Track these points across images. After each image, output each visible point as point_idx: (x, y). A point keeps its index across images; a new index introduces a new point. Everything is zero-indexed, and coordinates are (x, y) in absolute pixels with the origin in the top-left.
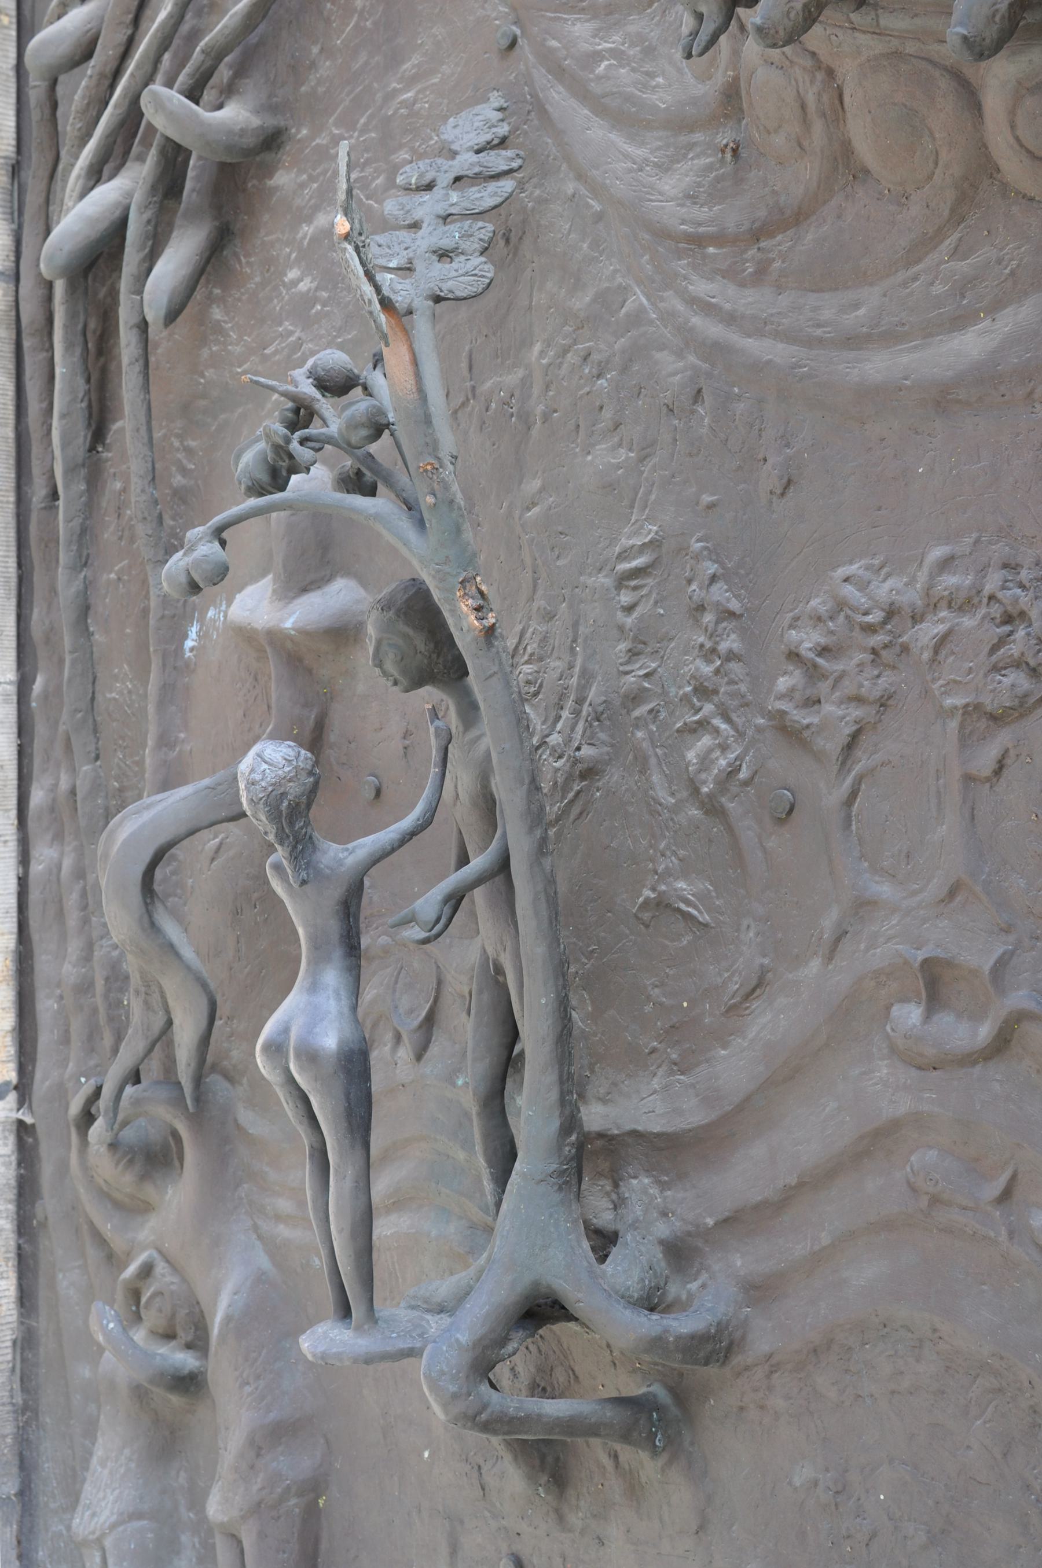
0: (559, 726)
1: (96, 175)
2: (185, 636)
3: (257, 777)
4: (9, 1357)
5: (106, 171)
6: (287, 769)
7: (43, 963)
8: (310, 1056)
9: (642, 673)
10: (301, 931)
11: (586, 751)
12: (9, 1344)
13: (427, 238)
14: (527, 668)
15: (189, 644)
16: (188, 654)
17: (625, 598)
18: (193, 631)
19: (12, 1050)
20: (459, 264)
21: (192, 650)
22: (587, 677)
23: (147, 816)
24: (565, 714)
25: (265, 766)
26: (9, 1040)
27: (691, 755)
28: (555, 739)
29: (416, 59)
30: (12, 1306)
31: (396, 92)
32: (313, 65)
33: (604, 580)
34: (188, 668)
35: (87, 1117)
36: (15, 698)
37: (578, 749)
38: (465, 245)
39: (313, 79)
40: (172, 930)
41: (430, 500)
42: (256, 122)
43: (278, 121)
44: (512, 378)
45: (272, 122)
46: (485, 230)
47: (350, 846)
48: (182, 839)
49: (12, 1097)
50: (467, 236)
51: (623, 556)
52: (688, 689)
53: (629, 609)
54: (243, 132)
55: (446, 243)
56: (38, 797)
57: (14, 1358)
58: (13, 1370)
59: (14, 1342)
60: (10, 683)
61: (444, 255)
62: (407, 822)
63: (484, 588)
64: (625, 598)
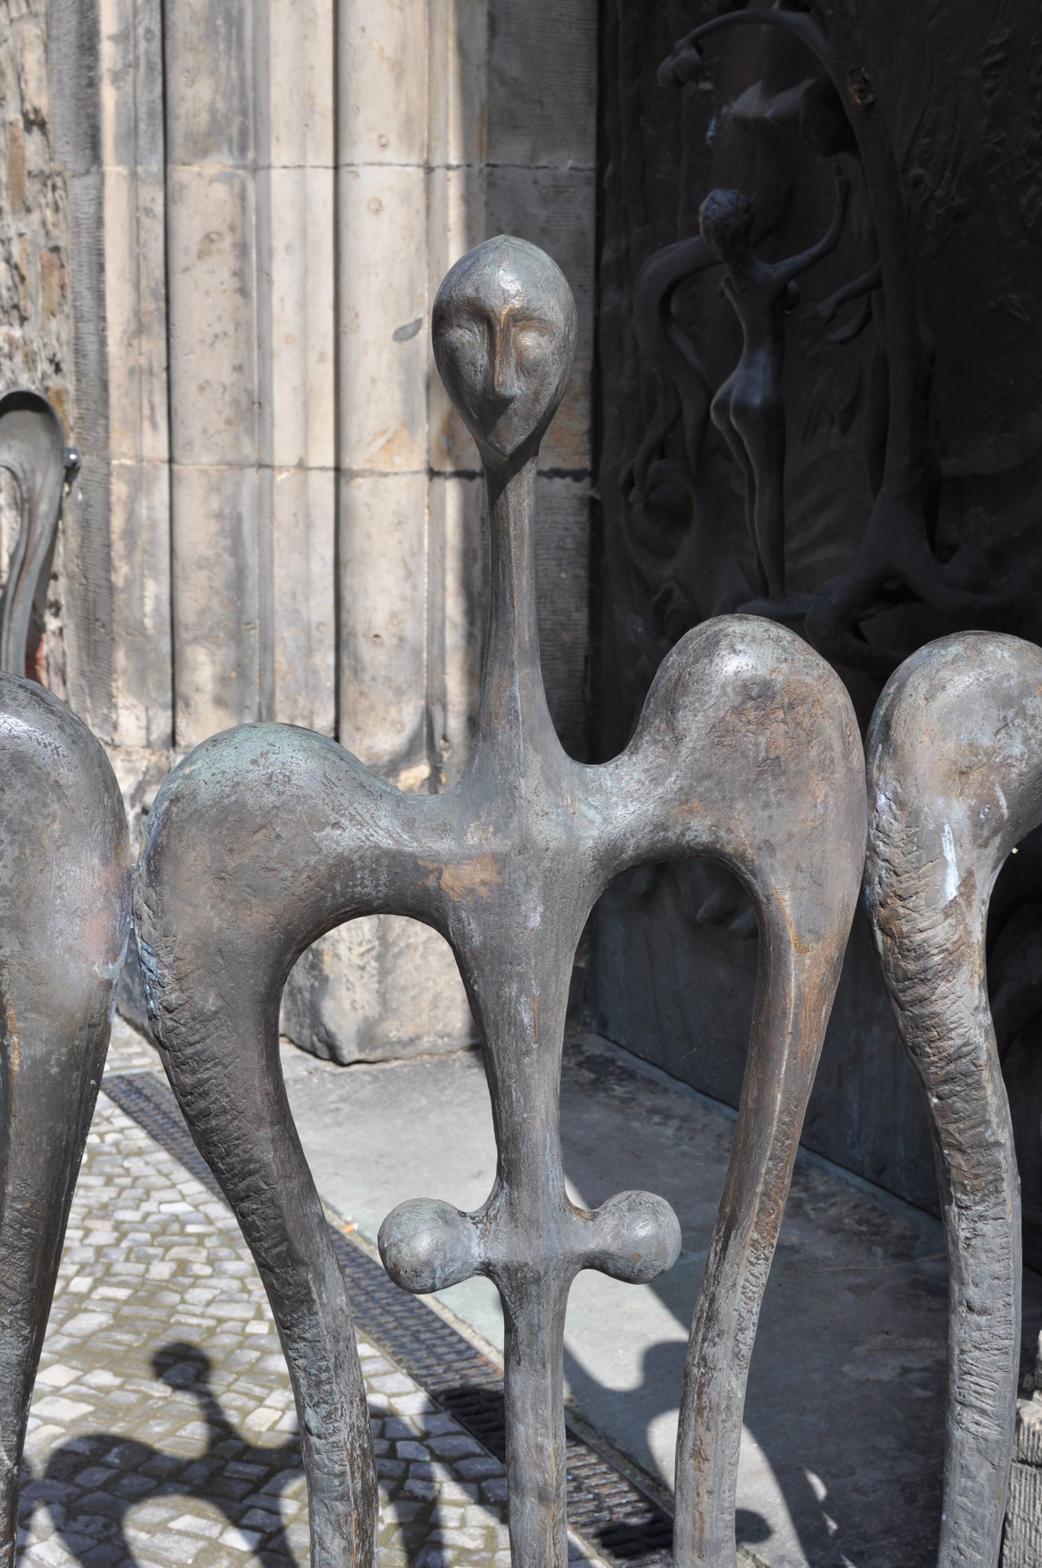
0: (943, 183)
2: (707, 129)
3: (709, 213)
4: (582, 668)
6: (730, 208)
8: (742, 410)
9: (996, 140)
10: (743, 325)
12: (582, 658)
14: (925, 141)
15: (710, 133)
16: (709, 142)
17: (988, 85)
18: (713, 124)
19: (588, 447)
21: (712, 138)
24: (947, 174)
25: (715, 206)
26: (585, 438)
27: (1024, 201)
28: (940, 193)
30: (585, 632)
35: (630, 483)
36: (594, 181)
37: (953, 199)
40: (683, 343)
41: (830, 12)
47: (776, 265)
48: (430, 99)
49: (587, 481)
52: (1024, 151)
53: (990, 93)
56: (607, 254)
57: (586, 671)
58: (585, 677)
59: (586, 658)
60: (591, 170)
62: (815, 249)
63: (866, 76)
64: (988, 85)
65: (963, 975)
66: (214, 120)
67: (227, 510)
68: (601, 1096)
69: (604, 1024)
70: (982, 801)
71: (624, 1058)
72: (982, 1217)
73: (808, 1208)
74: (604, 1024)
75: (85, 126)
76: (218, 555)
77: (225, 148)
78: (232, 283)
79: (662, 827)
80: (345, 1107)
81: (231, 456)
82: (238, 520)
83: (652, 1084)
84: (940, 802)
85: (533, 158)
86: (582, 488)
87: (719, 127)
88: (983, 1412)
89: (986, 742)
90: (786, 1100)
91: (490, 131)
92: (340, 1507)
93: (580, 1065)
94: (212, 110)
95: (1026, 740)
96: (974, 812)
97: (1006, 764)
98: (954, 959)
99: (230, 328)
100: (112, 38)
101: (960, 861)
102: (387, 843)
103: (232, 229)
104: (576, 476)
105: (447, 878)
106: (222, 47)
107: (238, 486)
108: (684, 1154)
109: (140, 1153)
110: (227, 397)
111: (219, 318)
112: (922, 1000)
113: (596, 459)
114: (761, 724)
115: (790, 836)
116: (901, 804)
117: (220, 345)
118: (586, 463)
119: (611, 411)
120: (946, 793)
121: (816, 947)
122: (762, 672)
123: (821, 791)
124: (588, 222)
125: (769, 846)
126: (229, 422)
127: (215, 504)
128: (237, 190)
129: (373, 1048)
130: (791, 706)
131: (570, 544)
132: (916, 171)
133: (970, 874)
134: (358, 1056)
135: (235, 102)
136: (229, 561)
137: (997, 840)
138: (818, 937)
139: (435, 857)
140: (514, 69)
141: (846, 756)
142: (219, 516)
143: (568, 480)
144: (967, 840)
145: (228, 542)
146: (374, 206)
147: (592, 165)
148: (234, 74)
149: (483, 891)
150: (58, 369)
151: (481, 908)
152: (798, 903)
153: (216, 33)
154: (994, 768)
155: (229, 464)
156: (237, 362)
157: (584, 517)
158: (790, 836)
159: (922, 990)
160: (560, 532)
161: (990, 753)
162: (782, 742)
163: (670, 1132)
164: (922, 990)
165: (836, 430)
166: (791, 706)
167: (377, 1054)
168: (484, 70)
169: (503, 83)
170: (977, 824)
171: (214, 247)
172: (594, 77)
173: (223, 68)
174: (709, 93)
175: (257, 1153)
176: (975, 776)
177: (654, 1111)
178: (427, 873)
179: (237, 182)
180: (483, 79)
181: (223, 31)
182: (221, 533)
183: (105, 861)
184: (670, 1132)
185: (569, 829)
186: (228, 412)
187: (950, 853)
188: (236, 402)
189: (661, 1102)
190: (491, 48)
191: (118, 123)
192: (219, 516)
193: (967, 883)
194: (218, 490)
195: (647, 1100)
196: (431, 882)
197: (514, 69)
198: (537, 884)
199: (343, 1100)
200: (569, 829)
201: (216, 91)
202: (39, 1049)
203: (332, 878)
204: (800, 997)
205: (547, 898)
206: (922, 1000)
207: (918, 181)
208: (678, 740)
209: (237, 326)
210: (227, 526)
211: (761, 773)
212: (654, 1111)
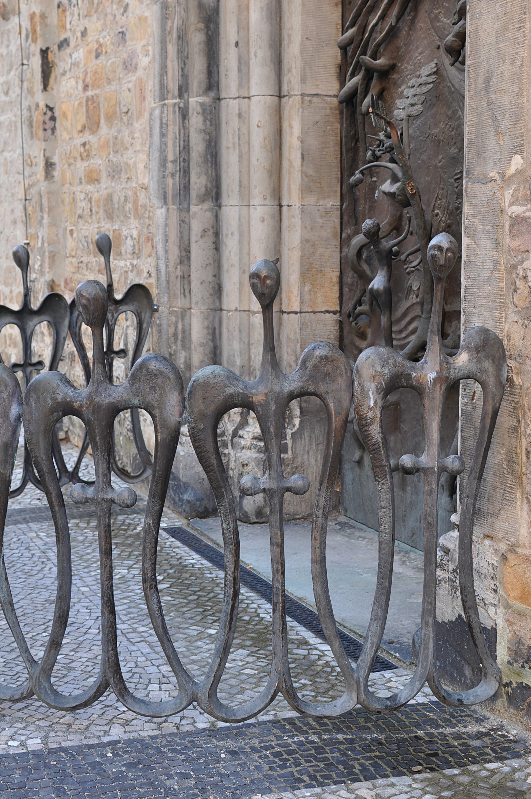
1: (353, 75)
5: (356, 73)
7: (345, 278)
11: (448, 221)
13: (409, 101)
15: (376, 195)
20: (416, 107)
22: (449, 204)
23: (359, 238)
26: (337, 299)
28: (443, 219)
29: (421, 49)
31: (417, 57)
32: (401, 48)
33: (453, 180)
34: (376, 201)
38: (418, 102)
39: (401, 51)
42: (388, 63)
43: (394, 62)
44: (437, 131)
45: (392, 62)
46: (423, 98)
49: (338, 314)
50: (418, 100)
51: (455, 175)
53: (457, 187)
54: (384, 66)
55: (413, 102)
56: (344, 235)
61: (412, 105)
65: (376, 424)
66: (206, 190)
67: (210, 326)
68: (342, 533)
69: (346, 511)
70: (379, 383)
71: (352, 522)
72: (383, 484)
73: (407, 563)
74: (346, 511)
75: (161, 191)
76: (207, 342)
77: (210, 200)
78: (213, 246)
79: (303, 388)
80: (251, 535)
81: (212, 307)
82: (215, 329)
83: (361, 530)
84: (369, 384)
85: (317, 202)
86: (337, 317)
87: (379, 193)
88: (386, 533)
89: (379, 370)
90: (333, 452)
91: (302, 193)
92: (231, 547)
93: (336, 524)
94: (206, 187)
95: (389, 370)
96: (377, 386)
97: (384, 375)
98: (373, 420)
99: (212, 262)
100: (171, 162)
101: (374, 398)
102: (241, 391)
103: (213, 227)
104: (334, 313)
105: (254, 399)
106: (209, 165)
107: (214, 317)
108: (368, 549)
109: (178, 547)
110: (211, 286)
111: (208, 259)
112: (366, 431)
113: (341, 307)
114: (325, 365)
115: (333, 391)
116: (360, 384)
117: (208, 268)
118: (338, 308)
119: (346, 290)
120: (370, 382)
121: (339, 416)
122: (325, 353)
123: (340, 380)
124: (338, 224)
125: (327, 393)
126: (211, 295)
127: (206, 324)
128: (214, 214)
129: (262, 518)
130: (332, 361)
131: (332, 337)
132: (437, 211)
133: (376, 400)
134: (256, 520)
135: (214, 183)
136: (211, 344)
137: (383, 393)
138: (340, 414)
139: (251, 394)
140: (310, 172)
141: (346, 373)
142: (207, 328)
143: (331, 314)
144: (375, 393)
145: (211, 337)
146: (262, 219)
147: (339, 204)
148: (214, 174)
149: (262, 401)
150: (150, 276)
151: (262, 405)
152: (334, 406)
153: (208, 160)
154: (381, 376)
155: (211, 310)
156: (214, 274)
157: (337, 327)
158: (333, 391)
159: (366, 428)
160: (329, 333)
161: (380, 373)
162: (330, 369)
163: (364, 543)
164: (366, 428)
165: (415, 296)
166: (332, 361)
167: (263, 520)
168: (300, 173)
169: (307, 177)
170: (377, 389)
171: (206, 234)
172: (339, 173)
173: (210, 172)
174: (376, 181)
175: (212, 461)
176: (377, 378)
177: (360, 537)
178: (250, 397)
179: (214, 211)
180: (300, 175)
181: (210, 160)
182: (208, 334)
183: (179, 395)
184: (364, 543)
185: (281, 388)
186: (211, 291)
187: (371, 396)
188: (214, 288)
189: (363, 534)
190: (302, 165)
191: (173, 191)
192: (207, 328)
193: (375, 402)
194: (207, 319)
195: (357, 534)
196: (250, 399)
197: (310, 172)
198: (274, 400)
199: (250, 533)
200: (281, 388)
201: (207, 180)
202: (164, 436)
203: (229, 398)
204: (336, 428)
205: (276, 403)
206: (366, 431)
207: (437, 215)
208: (306, 368)
209: (214, 261)
210: (211, 332)
211: (325, 376)
212: (360, 537)
